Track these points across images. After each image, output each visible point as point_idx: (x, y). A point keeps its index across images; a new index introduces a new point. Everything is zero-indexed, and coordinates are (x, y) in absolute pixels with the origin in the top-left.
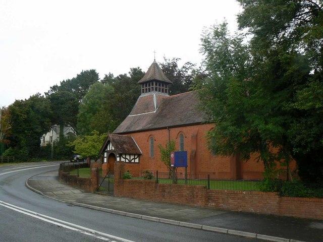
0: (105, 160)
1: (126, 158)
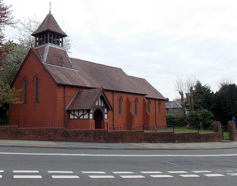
1: (74, 115)
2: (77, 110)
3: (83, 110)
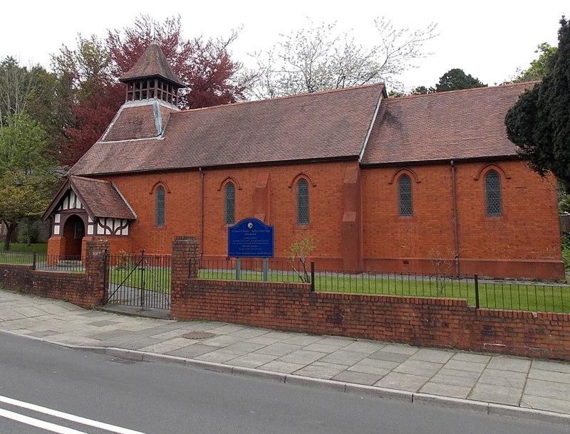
0: (57, 230)
1: (105, 227)
2: (118, 219)
3: (122, 220)
